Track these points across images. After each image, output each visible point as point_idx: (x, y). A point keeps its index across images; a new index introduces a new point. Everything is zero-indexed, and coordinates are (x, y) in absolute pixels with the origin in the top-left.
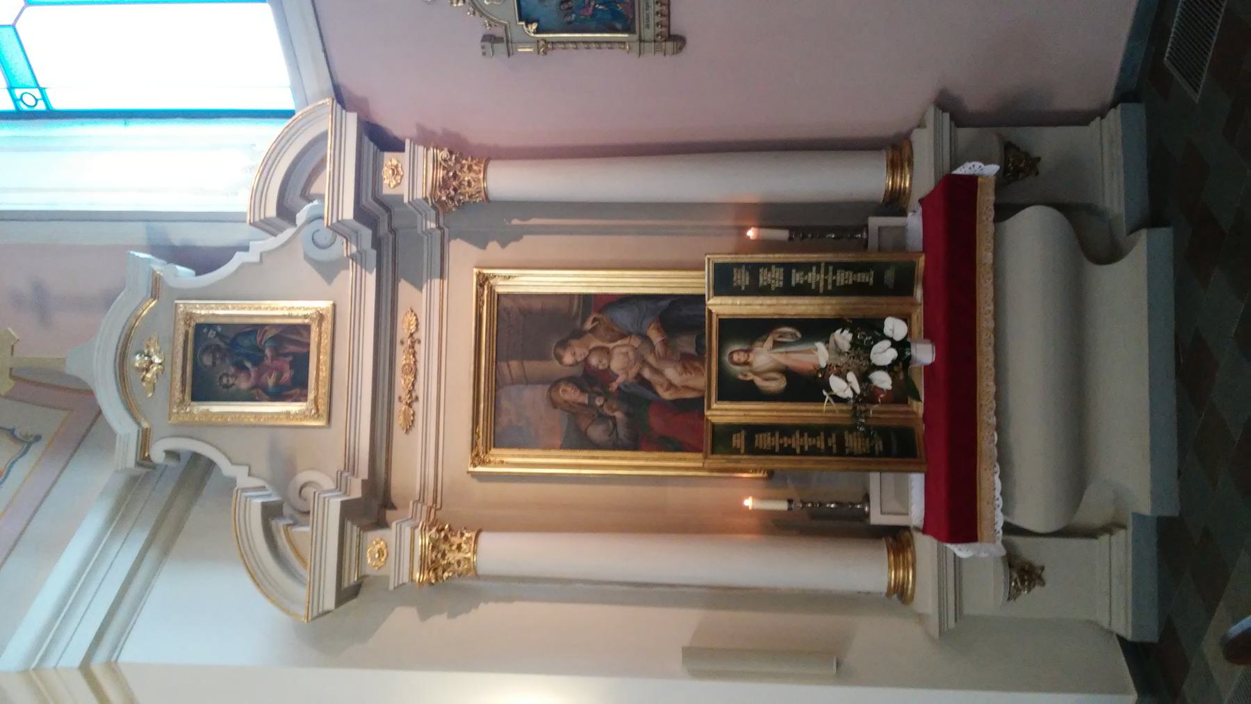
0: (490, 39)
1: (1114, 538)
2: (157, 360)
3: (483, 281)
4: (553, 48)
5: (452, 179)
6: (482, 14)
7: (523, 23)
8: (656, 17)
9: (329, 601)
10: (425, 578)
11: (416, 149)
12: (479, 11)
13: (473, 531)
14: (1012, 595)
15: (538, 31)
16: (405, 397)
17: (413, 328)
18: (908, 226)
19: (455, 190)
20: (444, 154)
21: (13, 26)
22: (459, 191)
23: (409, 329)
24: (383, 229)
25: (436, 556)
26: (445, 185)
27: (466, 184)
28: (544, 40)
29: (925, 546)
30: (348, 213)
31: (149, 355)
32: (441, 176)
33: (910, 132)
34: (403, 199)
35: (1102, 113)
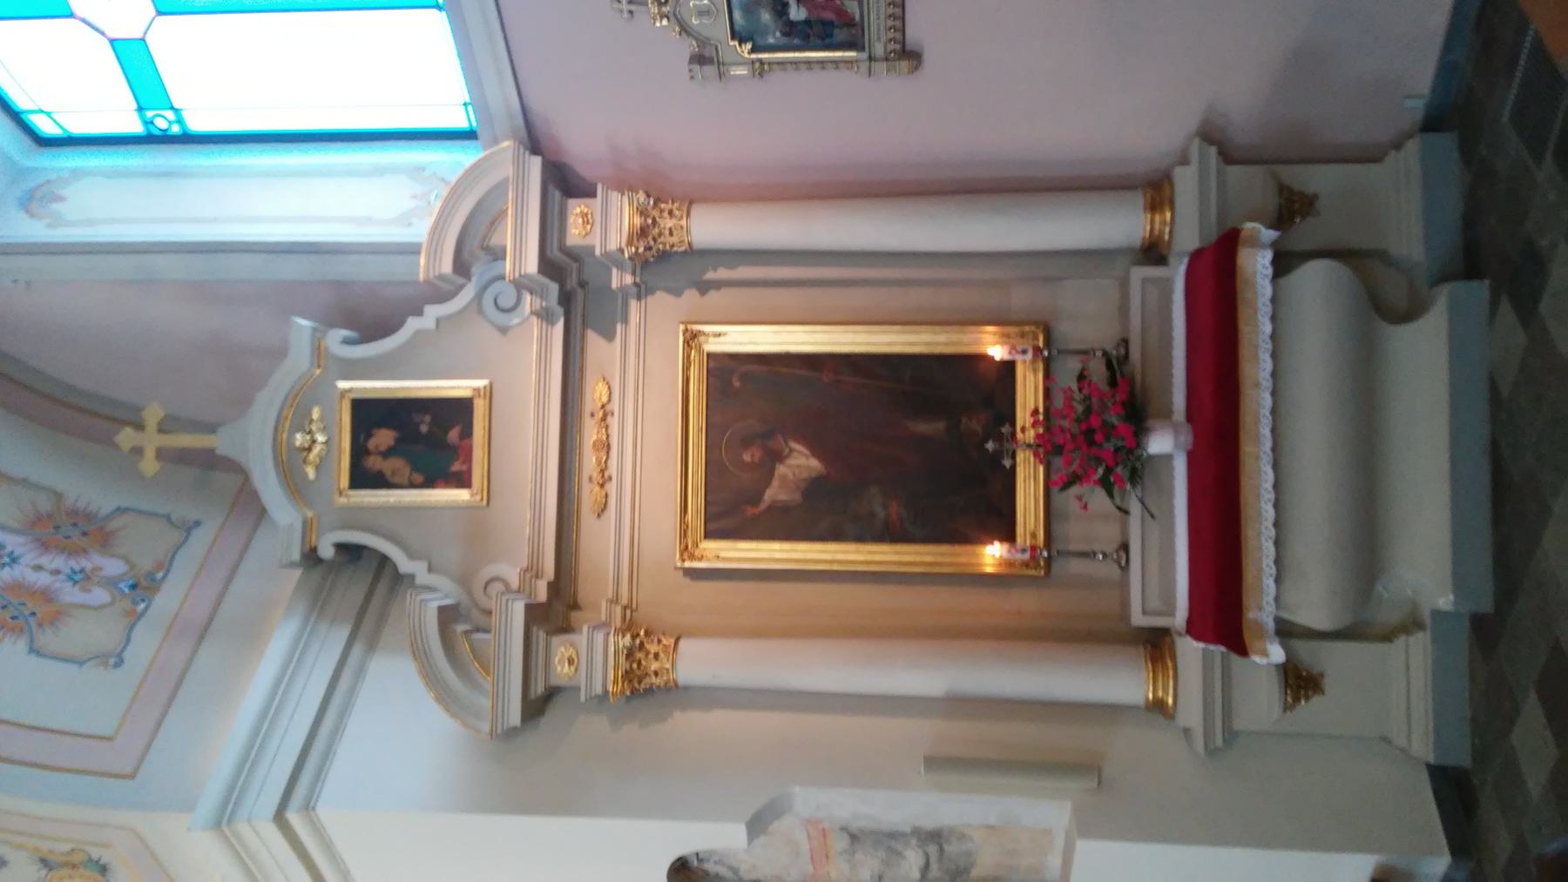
0: (700, 59)
1: (1412, 639)
2: (321, 438)
3: (692, 338)
4: (770, 70)
5: (651, 227)
6: (689, 34)
7: (736, 43)
8: (888, 32)
9: (515, 716)
10: (619, 690)
11: (609, 196)
12: (686, 31)
13: (671, 636)
14: (1287, 708)
15: (753, 51)
16: (596, 475)
17: (605, 399)
18: (1243, 232)
19: (655, 240)
20: (642, 197)
21: (143, 39)
22: (659, 240)
23: (600, 399)
24: (572, 282)
25: (631, 667)
26: (643, 232)
27: (667, 232)
28: (761, 62)
29: (1190, 650)
30: (531, 265)
31: (310, 432)
32: (639, 226)
33: (1172, 166)
34: (594, 250)
35: (1397, 146)
